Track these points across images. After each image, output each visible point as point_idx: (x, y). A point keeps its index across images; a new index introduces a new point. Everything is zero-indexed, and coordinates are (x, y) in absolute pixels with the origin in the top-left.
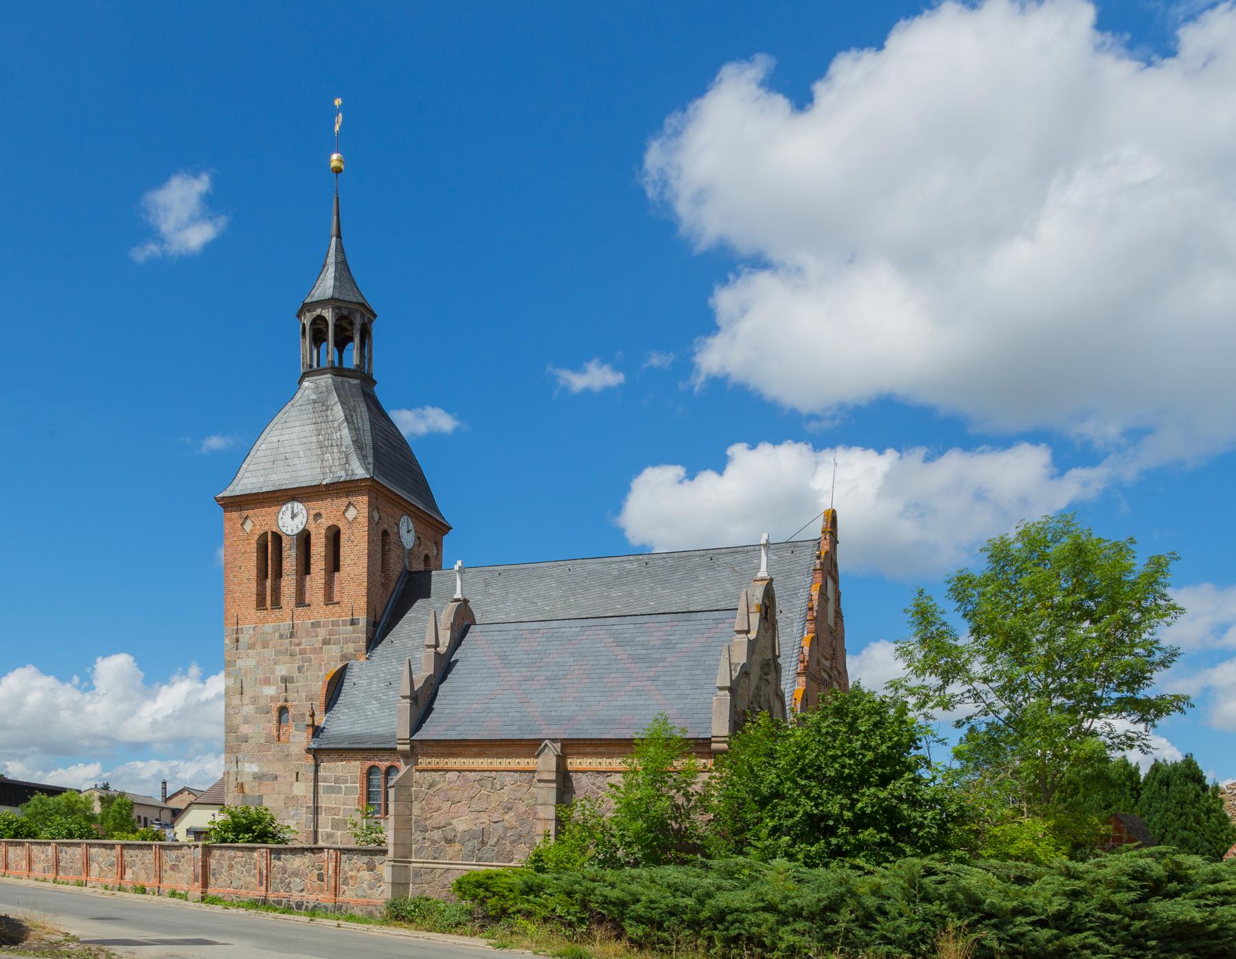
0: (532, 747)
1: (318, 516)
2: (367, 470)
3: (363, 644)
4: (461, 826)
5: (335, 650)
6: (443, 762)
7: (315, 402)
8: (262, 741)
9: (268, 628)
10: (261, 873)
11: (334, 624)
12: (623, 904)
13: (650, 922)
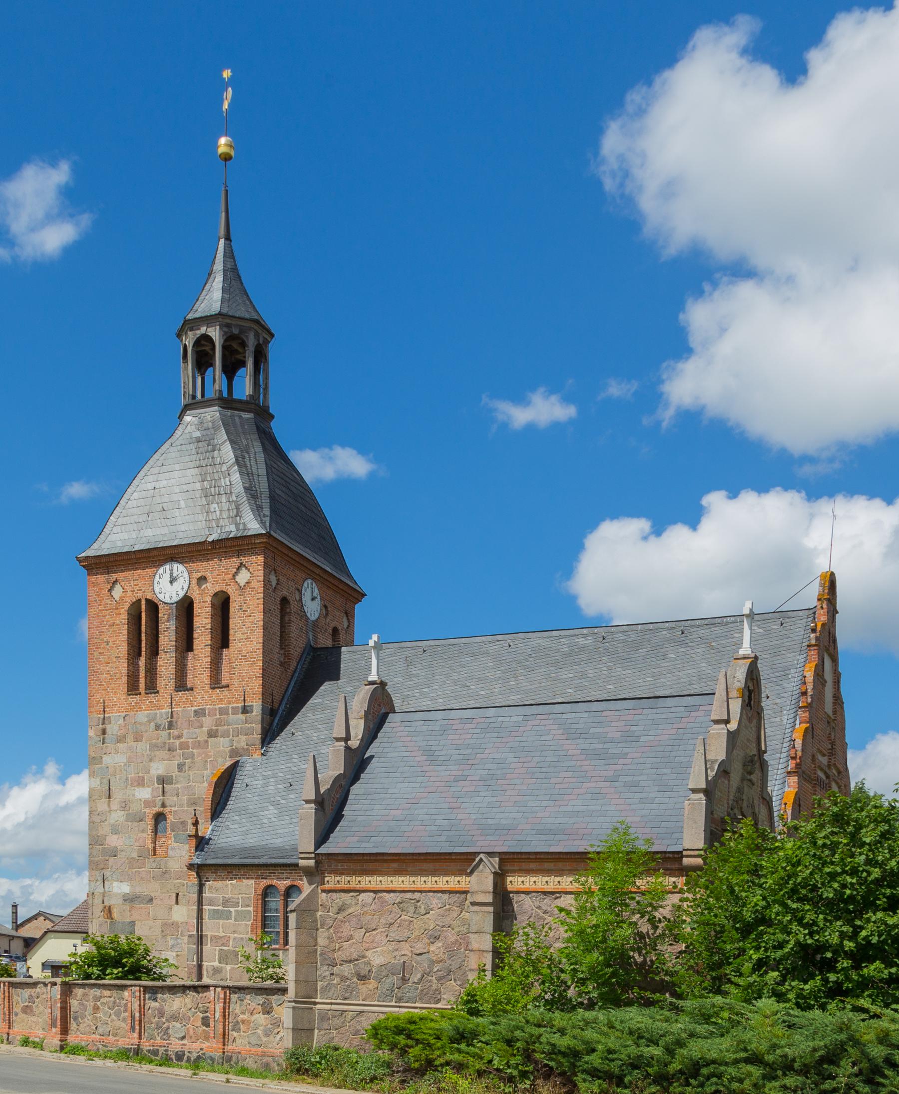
0: (463, 862)
1: (202, 579)
2: (262, 523)
3: (257, 737)
4: (376, 959)
5: (222, 744)
6: (355, 881)
7: (198, 440)
9: (142, 716)
10: (132, 1017)
11: (223, 711)
12: (575, 1054)
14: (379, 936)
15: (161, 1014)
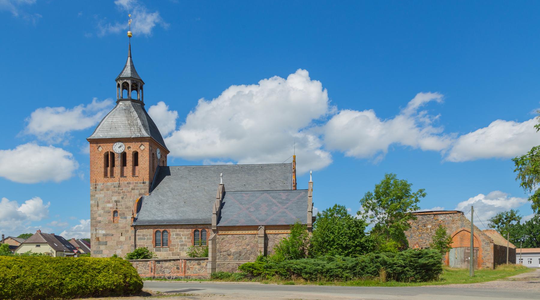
0: (256, 228)
1: (129, 147)
2: (148, 134)
3: (148, 190)
4: (233, 250)
5: (136, 192)
6: (226, 232)
7: (125, 110)
8: (107, 222)
9: (109, 184)
10: (152, 269)
11: (136, 183)
12: (301, 269)
13: (310, 273)
14: (233, 245)
15: (162, 267)
